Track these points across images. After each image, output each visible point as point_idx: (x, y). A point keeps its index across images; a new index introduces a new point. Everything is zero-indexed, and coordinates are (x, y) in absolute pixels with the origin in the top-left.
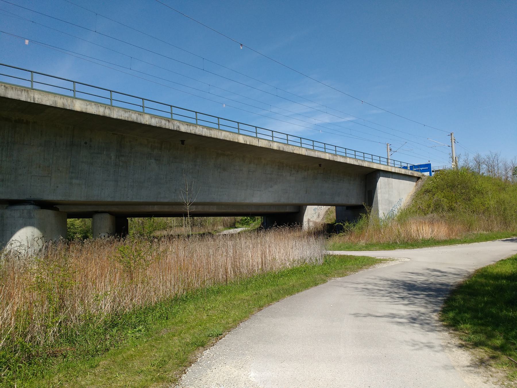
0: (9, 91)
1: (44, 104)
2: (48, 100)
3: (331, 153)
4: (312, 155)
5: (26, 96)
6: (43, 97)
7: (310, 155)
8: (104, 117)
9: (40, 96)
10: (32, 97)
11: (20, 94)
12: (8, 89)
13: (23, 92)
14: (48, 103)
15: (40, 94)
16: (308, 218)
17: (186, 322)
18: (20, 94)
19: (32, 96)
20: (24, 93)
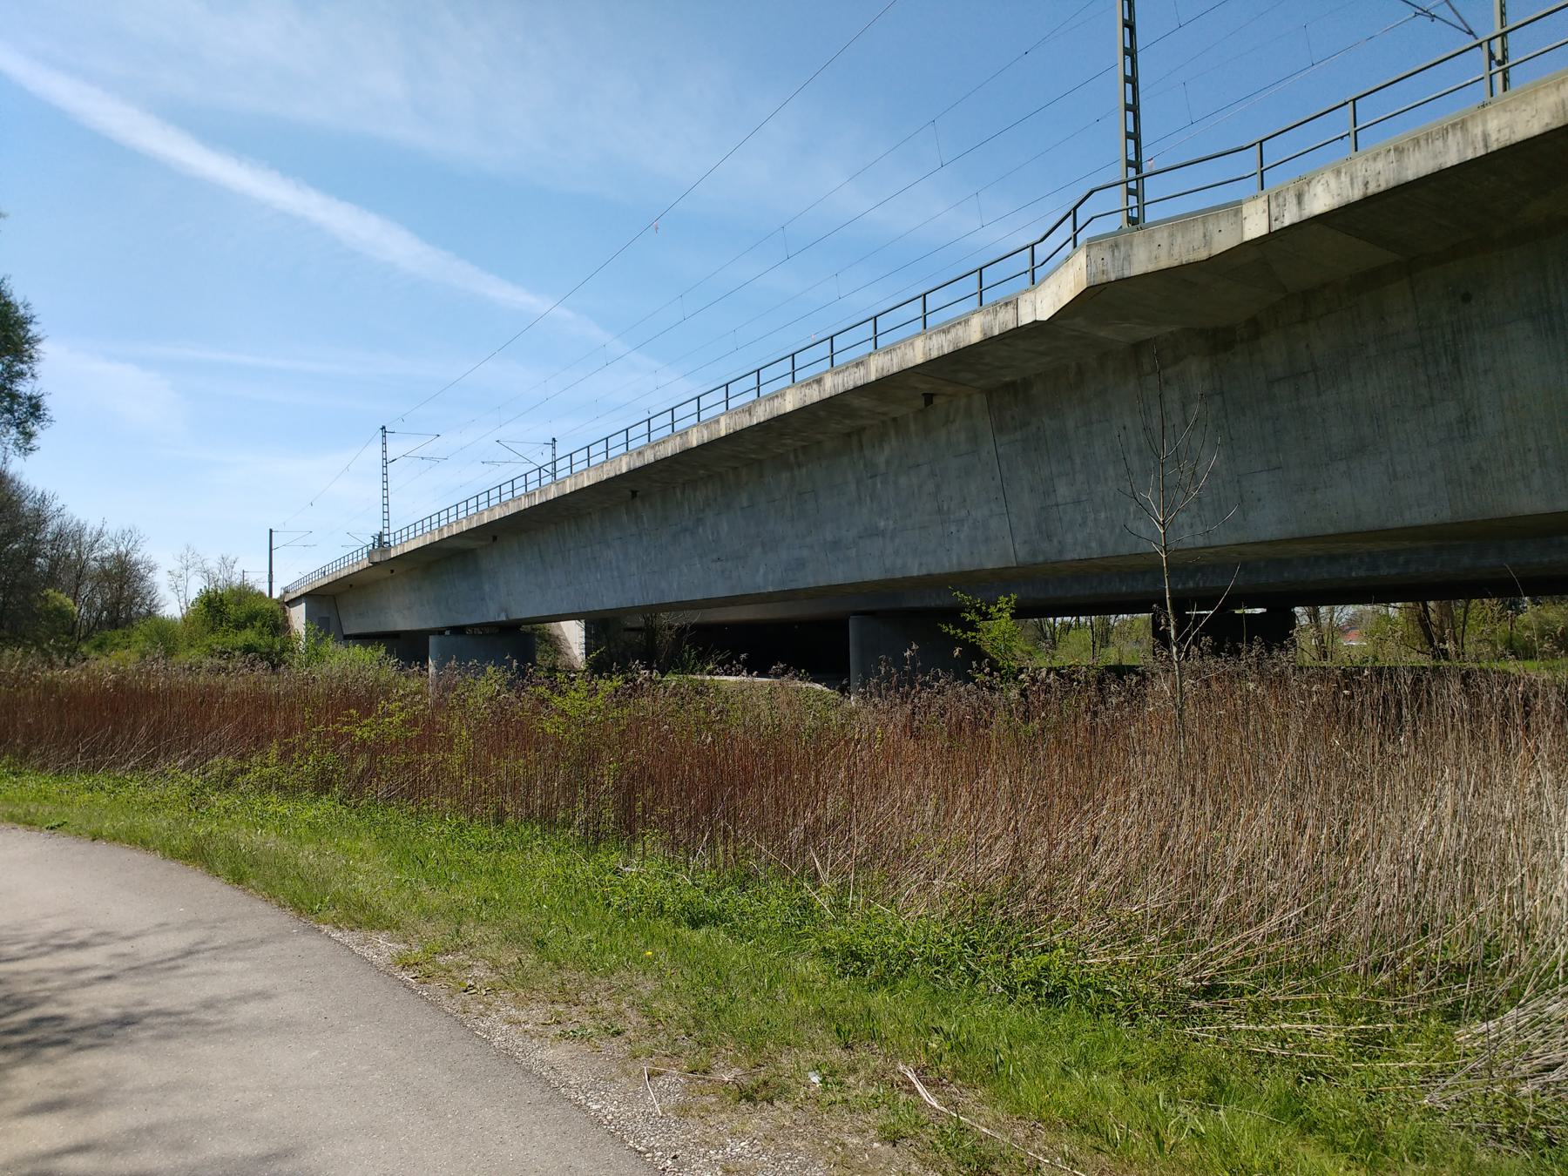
0: (1409, 158)
1: (1519, 140)
2: (1533, 117)
3: (1225, 206)
4: (579, 608)
5: (1458, 144)
6: (1518, 111)
7: (579, 608)
8: (985, 343)
9: (1505, 118)
10: (1480, 138)
11: (1442, 149)
12: (1406, 152)
13: (1450, 134)
14: (1536, 129)
15: (1506, 111)
16: (220, 557)
17: (347, 1104)
18: (1442, 149)
19: (1479, 134)
20: (1454, 135)
